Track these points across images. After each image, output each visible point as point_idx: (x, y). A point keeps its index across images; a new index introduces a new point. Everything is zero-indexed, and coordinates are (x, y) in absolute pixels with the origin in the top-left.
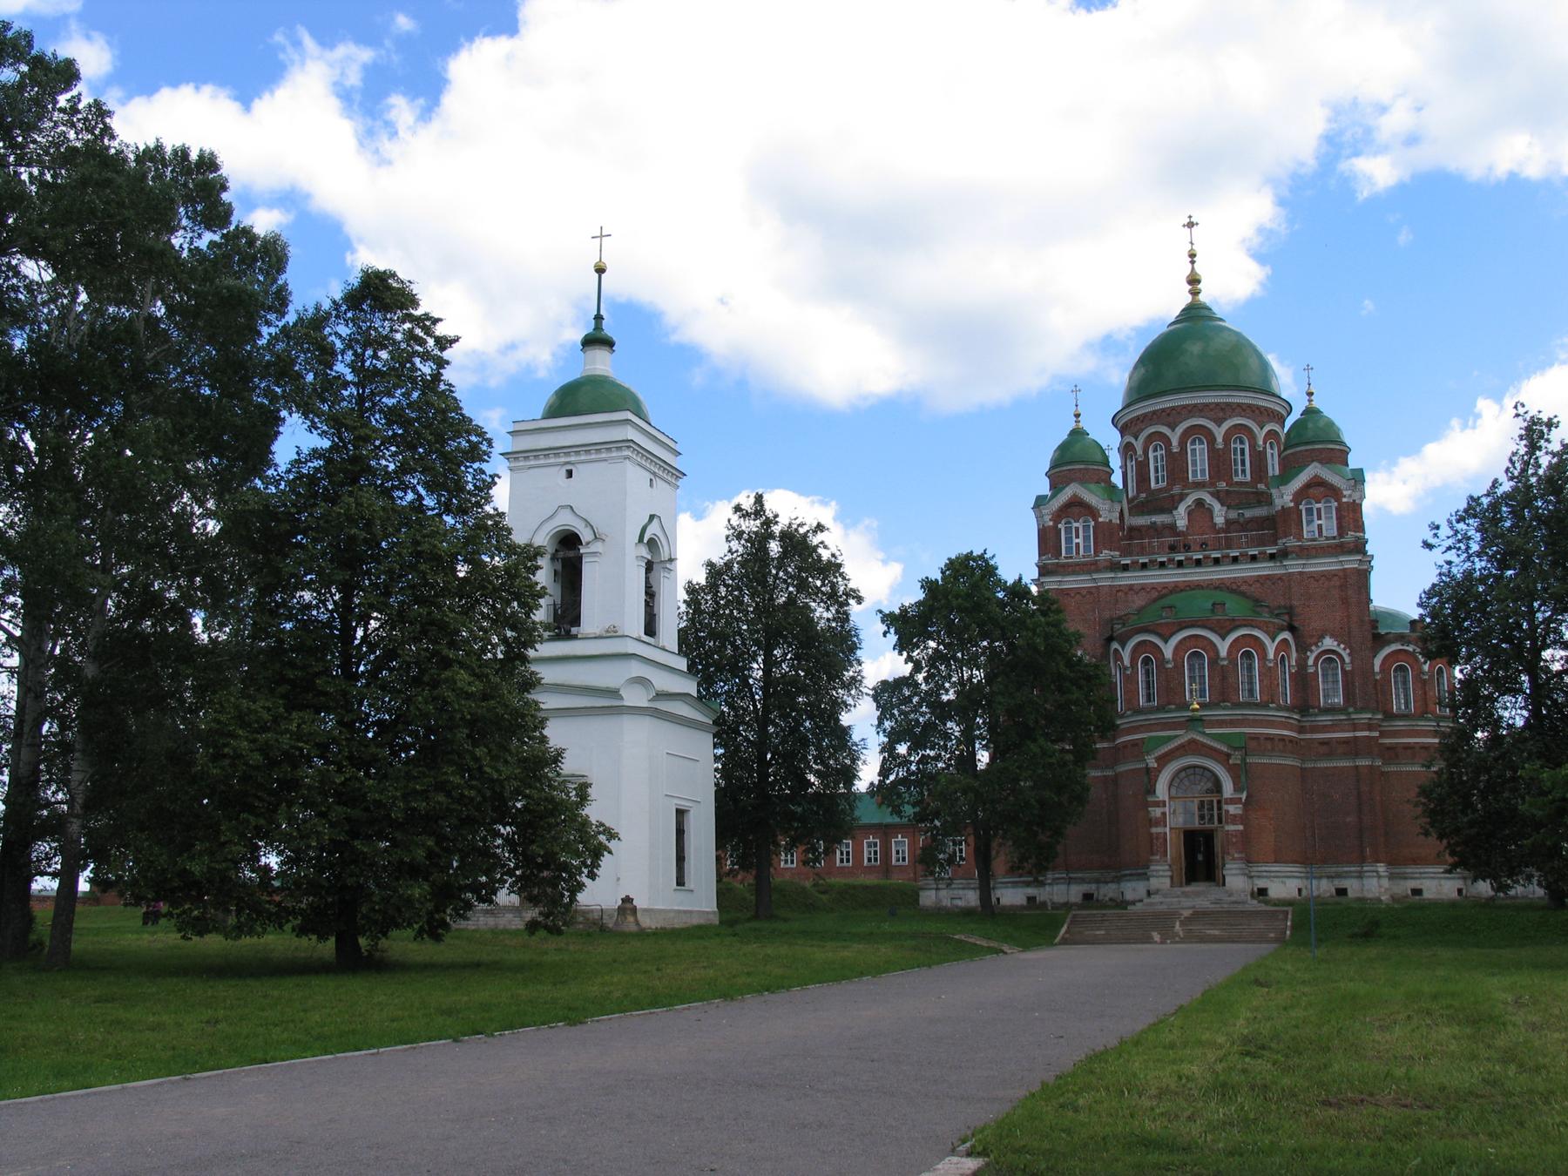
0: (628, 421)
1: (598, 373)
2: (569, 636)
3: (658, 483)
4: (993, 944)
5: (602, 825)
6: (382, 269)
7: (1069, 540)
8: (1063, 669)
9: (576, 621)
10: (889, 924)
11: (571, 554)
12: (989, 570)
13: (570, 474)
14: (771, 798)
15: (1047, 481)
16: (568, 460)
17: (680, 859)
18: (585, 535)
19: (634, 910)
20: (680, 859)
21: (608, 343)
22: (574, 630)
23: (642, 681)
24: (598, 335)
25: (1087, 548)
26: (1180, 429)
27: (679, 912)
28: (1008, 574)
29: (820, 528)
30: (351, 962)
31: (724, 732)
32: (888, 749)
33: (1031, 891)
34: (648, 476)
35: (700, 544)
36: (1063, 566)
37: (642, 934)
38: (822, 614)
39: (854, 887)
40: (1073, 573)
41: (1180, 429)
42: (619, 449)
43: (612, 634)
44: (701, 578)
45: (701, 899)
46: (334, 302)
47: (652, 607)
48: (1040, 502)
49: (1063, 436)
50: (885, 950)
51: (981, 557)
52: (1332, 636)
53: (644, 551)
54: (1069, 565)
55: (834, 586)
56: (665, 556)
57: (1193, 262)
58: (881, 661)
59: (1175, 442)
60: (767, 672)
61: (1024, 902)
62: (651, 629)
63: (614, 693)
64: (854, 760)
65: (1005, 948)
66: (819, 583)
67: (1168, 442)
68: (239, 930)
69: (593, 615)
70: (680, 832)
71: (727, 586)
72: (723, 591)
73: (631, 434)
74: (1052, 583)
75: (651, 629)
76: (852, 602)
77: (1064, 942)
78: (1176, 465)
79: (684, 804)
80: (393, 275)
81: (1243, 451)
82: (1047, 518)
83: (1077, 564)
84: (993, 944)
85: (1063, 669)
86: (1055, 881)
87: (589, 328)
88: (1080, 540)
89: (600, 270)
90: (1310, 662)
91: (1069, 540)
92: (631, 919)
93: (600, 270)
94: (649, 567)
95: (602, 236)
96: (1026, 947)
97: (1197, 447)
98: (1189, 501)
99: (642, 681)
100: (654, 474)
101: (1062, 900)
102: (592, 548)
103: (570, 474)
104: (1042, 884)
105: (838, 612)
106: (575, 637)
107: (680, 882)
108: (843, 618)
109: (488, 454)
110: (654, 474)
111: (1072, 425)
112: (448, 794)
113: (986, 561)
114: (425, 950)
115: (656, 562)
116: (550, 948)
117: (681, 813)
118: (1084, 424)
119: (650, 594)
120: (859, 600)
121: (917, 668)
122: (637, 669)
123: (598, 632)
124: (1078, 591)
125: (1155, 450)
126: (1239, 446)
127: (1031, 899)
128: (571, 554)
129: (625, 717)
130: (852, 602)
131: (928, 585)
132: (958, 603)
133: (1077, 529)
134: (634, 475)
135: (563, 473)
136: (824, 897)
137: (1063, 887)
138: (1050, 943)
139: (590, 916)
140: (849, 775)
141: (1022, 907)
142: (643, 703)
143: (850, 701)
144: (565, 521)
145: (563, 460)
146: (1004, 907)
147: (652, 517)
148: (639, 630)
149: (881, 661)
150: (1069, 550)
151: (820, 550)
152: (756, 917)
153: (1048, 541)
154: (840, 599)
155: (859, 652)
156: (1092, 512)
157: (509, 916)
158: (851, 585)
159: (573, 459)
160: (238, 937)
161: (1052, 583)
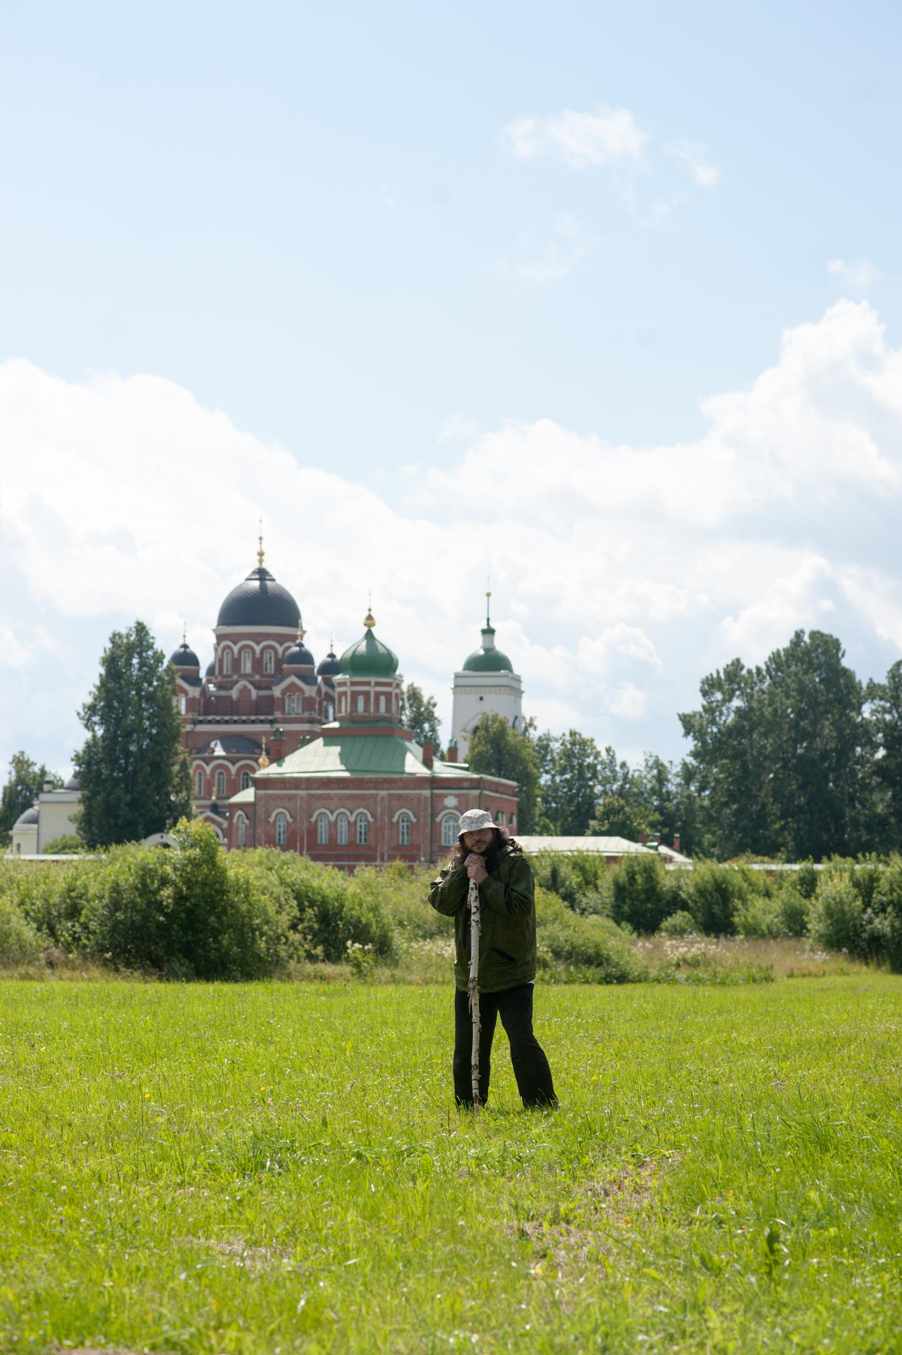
13: (481, 699)
78: (236, 664)
103: (481, 699)
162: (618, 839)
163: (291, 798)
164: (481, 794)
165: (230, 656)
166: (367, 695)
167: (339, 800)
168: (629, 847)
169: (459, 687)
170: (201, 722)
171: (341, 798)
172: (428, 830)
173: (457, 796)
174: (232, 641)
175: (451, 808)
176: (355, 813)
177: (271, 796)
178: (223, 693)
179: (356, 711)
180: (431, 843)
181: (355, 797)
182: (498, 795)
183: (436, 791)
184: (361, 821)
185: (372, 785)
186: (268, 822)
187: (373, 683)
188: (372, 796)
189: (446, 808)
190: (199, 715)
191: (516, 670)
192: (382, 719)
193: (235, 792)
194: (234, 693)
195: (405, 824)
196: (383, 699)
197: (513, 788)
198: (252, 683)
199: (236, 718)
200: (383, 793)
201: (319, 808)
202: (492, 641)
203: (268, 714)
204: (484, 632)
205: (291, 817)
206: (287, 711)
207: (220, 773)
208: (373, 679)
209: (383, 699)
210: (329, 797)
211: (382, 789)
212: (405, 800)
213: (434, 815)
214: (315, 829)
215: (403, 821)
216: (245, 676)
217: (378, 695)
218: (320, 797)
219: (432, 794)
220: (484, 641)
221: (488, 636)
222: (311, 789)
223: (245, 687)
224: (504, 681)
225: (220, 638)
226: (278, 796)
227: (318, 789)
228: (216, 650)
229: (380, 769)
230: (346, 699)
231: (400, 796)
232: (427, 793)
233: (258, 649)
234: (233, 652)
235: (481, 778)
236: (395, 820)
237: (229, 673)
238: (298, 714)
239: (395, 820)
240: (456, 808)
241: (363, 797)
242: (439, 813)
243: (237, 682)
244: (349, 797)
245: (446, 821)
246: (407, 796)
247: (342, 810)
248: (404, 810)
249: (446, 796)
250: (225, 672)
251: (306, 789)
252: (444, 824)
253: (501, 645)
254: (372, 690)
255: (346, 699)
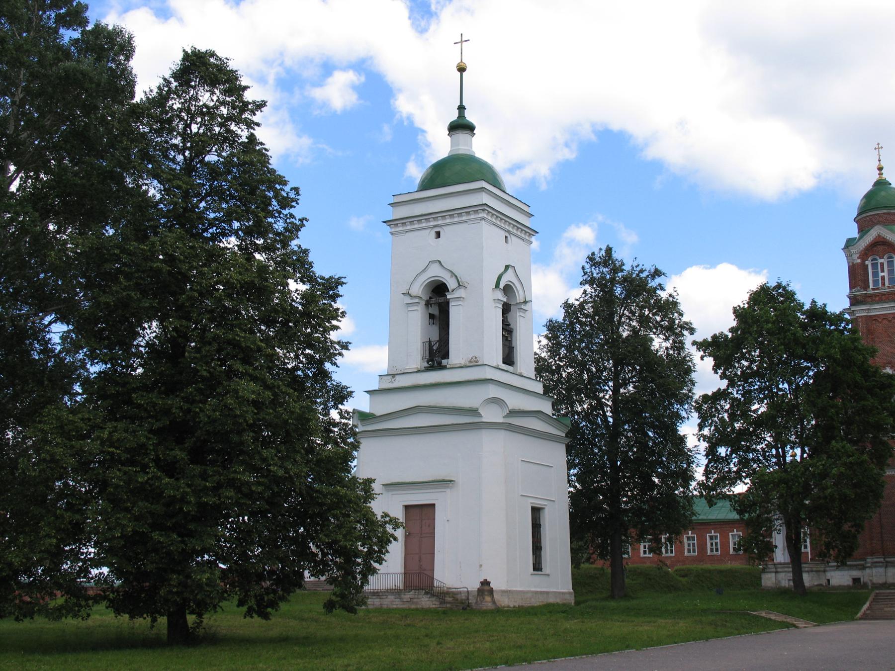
0: (482, 189)
1: (461, 152)
2: (441, 367)
3: (513, 240)
4: (789, 620)
5: (386, 515)
6: (203, 50)
7: (875, 274)
8: (859, 378)
9: (446, 355)
10: (729, 600)
11: (441, 300)
12: (789, 296)
13: (438, 235)
14: (619, 494)
15: (855, 225)
16: (436, 224)
17: (537, 548)
18: (451, 284)
19: (491, 591)
20: (537, 548)
21: (470, 128)
22: (444, 362)
23: (497, 401)
24: (461, 122)
27: (536, 592)
28: (136, 64)
29: (657, 273)
30: (182, 637)
31: (577, 444)
32: (711, 453)
33: (856, 573)
34: (503, 234)
35: (553, 290)
36: (871, 296)
37: (499, 611)
38: (659, 343)
39: (710, 571)
40: (881, 301)
42: (476, 212)
43: (474, 363)
44: (559, 315)
45: (558, 580)
46: (165, 79)
47: (510, 341)
48: (850, 243)
49: (868, 187)
50: (682, 625)
51: (779, 286)
53: (500, 296)
54: (876, 295)
55: (672, 321)
56: (520, 298)
58: (706, 377)
61: (850, 583)
62: (509, 358)
63: (474, 412)
64: (689, 463)
65: (800, 623)
66: (658, 318)
68: (58, 613)
69: (458, 352)
70: (536, 527)
71: (581, 323)
72: (578, 327)
73: (485, 199)
74: (862, 311)
75: (509, 358)
76: (686, 333)
77: (865, 617)
79: (538, 503)
80: (213, 54)
82: (855, 256)
83: (883, 294)
84: (789, 620)
85: (859, 378)
86: (874, 565)
87: (454, 116)
88: (885, 274)
89: (462, 69)
91: (875, 274)
92: (488, 599)
93: (462, 69)
94: (506, 309)
95: (462, 42)
96: (821, 620)
99: (497, 401)
100: (508, 231)
101: (881, 581)
102: (457, 294)
103: (438, 235)
104: (863, 568)
105: (674, 342)
106: (444, 368)
107: (537, 566)
108: (679, 346)
109: (296, 201)
110: (508, 231)
111: (875, 177)
112: (238, 490)
113: (784, 288)
114: (255, 625)
115: (510, 306)
116: (339, 624)
117: (536, 511)
118: (887, 176)
119: (508, 331)
120: (692, 331)
121: (732, 384)
122: (493, 391)
123: (463, 362)
124: (885, 317)
127: (856, 580)
128: (441, 300)
129: (484, 431)
130: (686, 333)
131: (738, 313)
132: (770, 324)
133: (882, 264)
134: (490, 235)
135: (433, 234)
136: (684, 580)
137: (882, 570)
138: (852, 618)
139: (459, 597)
140: (686, 477)
141: (849, 587)
142: (500, 420)
143: (683, 414)
144: (436, 273)
145: (432, 224)
146: (834, 588)
147: (507, 267)
148: (498, 359)
149: (706, 377)
150: (875, 282)
151: (659, 292)
152: (612, 597)
153: (857, 276)
154: (675, 330)
155: (693, 375)
157: (391, 597)
158: (685, 319)
159: (440, 222)
160: (59, 618)
161: (862, 311)
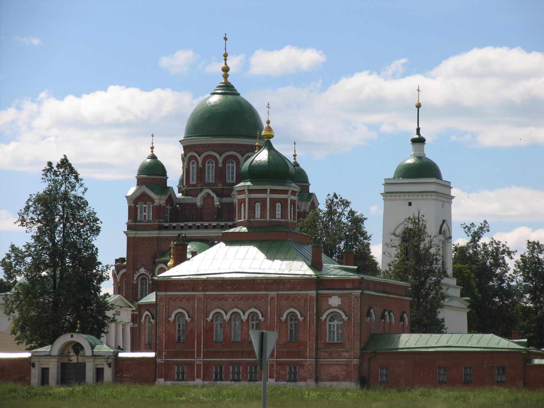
13: (410, 204)
25: (149, 216)
26: (223, 156)
41: (223, 156)
52: (145, 268)
57: (226, 60)
59: (220, 161)
60: (61, 273)
67: (217, 162)
78: (201, 172)
81: (233, 167)
90: (135, 278)
91: (141, 213)
97: (211, 165)
98: (202, 194)
100: (444, 201)
103: (410, 204)
125: (193, 164)
126: (231, 165)
133: (145, 208)
135: (407, 204)
145: (407, 198)
156: (152, 201)
159: (411, 198)
162: (490, 336)
163: (189, 299)
164: (362, 294)
165: (195, 165)
166: (284, 203)
167: (233, 300)
168: (72, 336)
169: (390, 193)
170: (166, 228)
171: (234, 298)
172: (314, 328)
173: (340, 296)
174: (197, 152)
175: (335, 308)
176: (247, 314)
177: (171, 297)
178: (189, 199)
179: (254, 217)
180: (317, 340)
181: (247, 298)
182: (385, 295)
183: (320, 292)
184: (252, 320)
185: (263, 287)
186: (169, 321)
187: (269, 190)
188: (262, 296)
189: (331, 307)
190: (166, 222)
191: (445, 177)
192: (279, 224)
193: (143, 296)
194: (198, 201)
195: (254, 323)
196: (278, 205)
197: (406, 288)
198: (214, 191)
199: (198, 224)
200: (273, 293)
201: (215, 309)
202: (423, 150)
203: (230, 221)
204: (414, 141)
205: (189, 317)
206: (139, 219)
207: (143, 279)
208: (269, 187)
209: (278, 205)
210: (223, 298)
211: (272, 290)
212: (293, 300)
213: (319, 314)
214: (211, 329)
215: (291, 320)
216: (209, 185)
217: (273, 202)
218: (215, 298)
219: (318, 294)
220: (415, 150)
221: (418, 145)
222: (207, 291)
223: (209, 195)
224: (432, 188)
225: (187, 148)
226: (177, 297)
227: (214, 290)
228: (183, 160)
229: (284, 273)
230: (245, 206)
231: (288, 296)
232: (313, 293)
233: (220, 160)
234: (198, 163)
235: (362, 278)
236: (284, 318)
237: (195, 183)
238: (149, 221)
239: (284, 318)
240: (339, 307)
241: (255, 297)
242: (323, 313)
243: (201, 190)
244: (242, 298)
245: (330, 321)
246: (295, 296)
247: (236, 310)
248: (292, 310)
249: (330, 296)
250: (191, 182)
251: (204, 290)
252: (328, 323)
253: (431, 153)
254: (268, 196)
255: (245, 206)
